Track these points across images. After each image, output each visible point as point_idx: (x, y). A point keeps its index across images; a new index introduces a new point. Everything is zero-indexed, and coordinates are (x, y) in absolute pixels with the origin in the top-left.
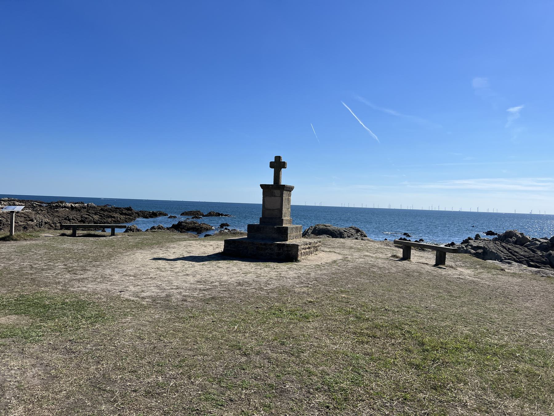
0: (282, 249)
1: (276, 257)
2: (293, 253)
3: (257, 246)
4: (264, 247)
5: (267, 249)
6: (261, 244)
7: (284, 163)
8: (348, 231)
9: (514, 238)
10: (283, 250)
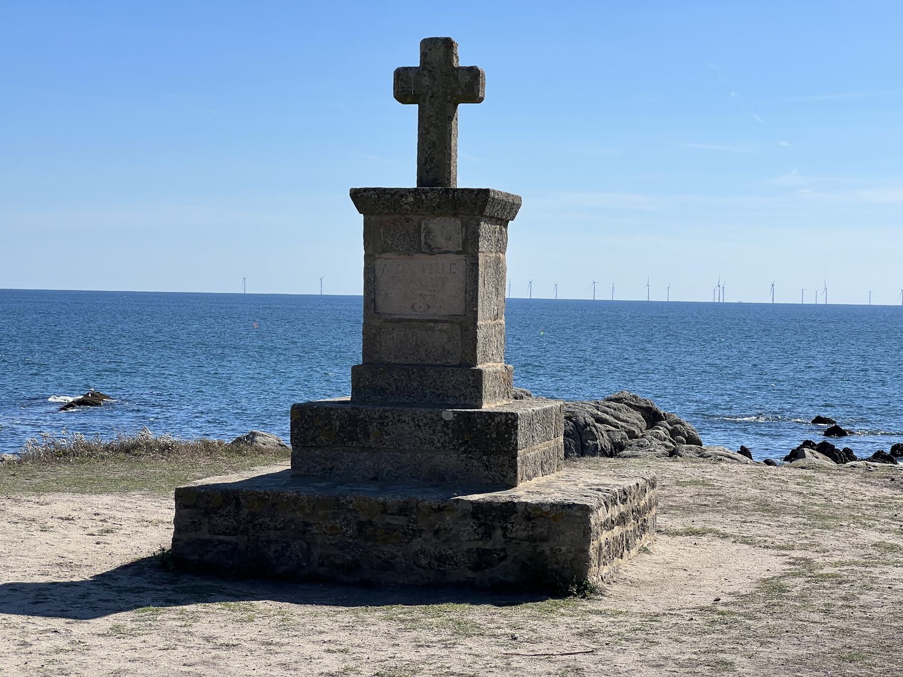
0: (499, 532)
1: (470, 574)
2: (564, 549)
3: (363, 518)
4: (400, 521)
5: (421, 531)
6: (385, 509)
7: (474, 74)
8: (611, 419)
10: (504, 535)
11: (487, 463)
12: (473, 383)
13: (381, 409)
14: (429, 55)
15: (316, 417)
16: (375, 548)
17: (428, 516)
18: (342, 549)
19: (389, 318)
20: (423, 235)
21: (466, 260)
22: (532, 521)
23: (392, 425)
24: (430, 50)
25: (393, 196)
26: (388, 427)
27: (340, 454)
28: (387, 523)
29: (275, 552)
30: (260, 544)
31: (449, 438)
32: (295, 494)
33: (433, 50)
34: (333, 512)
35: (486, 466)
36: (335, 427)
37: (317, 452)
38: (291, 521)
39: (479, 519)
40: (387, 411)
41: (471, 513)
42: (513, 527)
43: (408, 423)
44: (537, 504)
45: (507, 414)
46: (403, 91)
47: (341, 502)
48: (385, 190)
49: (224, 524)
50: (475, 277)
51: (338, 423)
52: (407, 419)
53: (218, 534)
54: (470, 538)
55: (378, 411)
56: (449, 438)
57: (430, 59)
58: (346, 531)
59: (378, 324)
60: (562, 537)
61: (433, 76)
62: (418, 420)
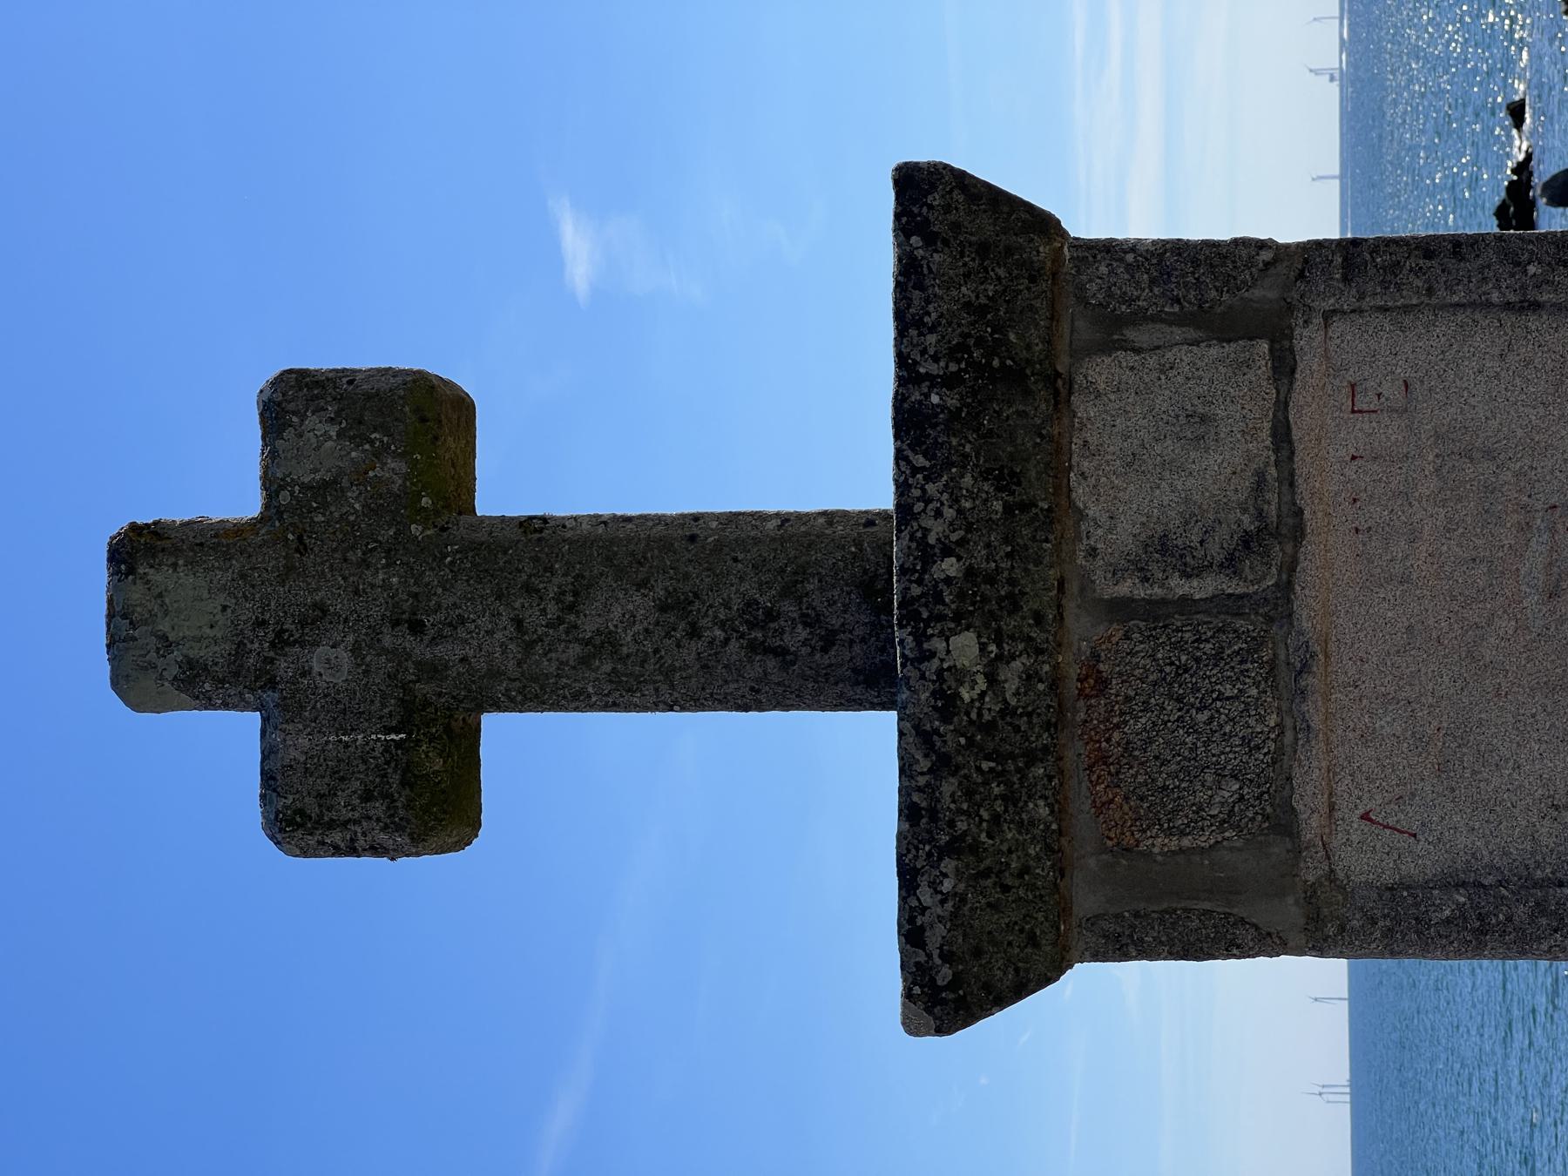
14: (197, 652)
20: (1180, 586)
21: (1328, 316)
24: (166, 644)
33: (164, 626)
46: (387, 796)
48: (909, 812)
61: (303, 624)
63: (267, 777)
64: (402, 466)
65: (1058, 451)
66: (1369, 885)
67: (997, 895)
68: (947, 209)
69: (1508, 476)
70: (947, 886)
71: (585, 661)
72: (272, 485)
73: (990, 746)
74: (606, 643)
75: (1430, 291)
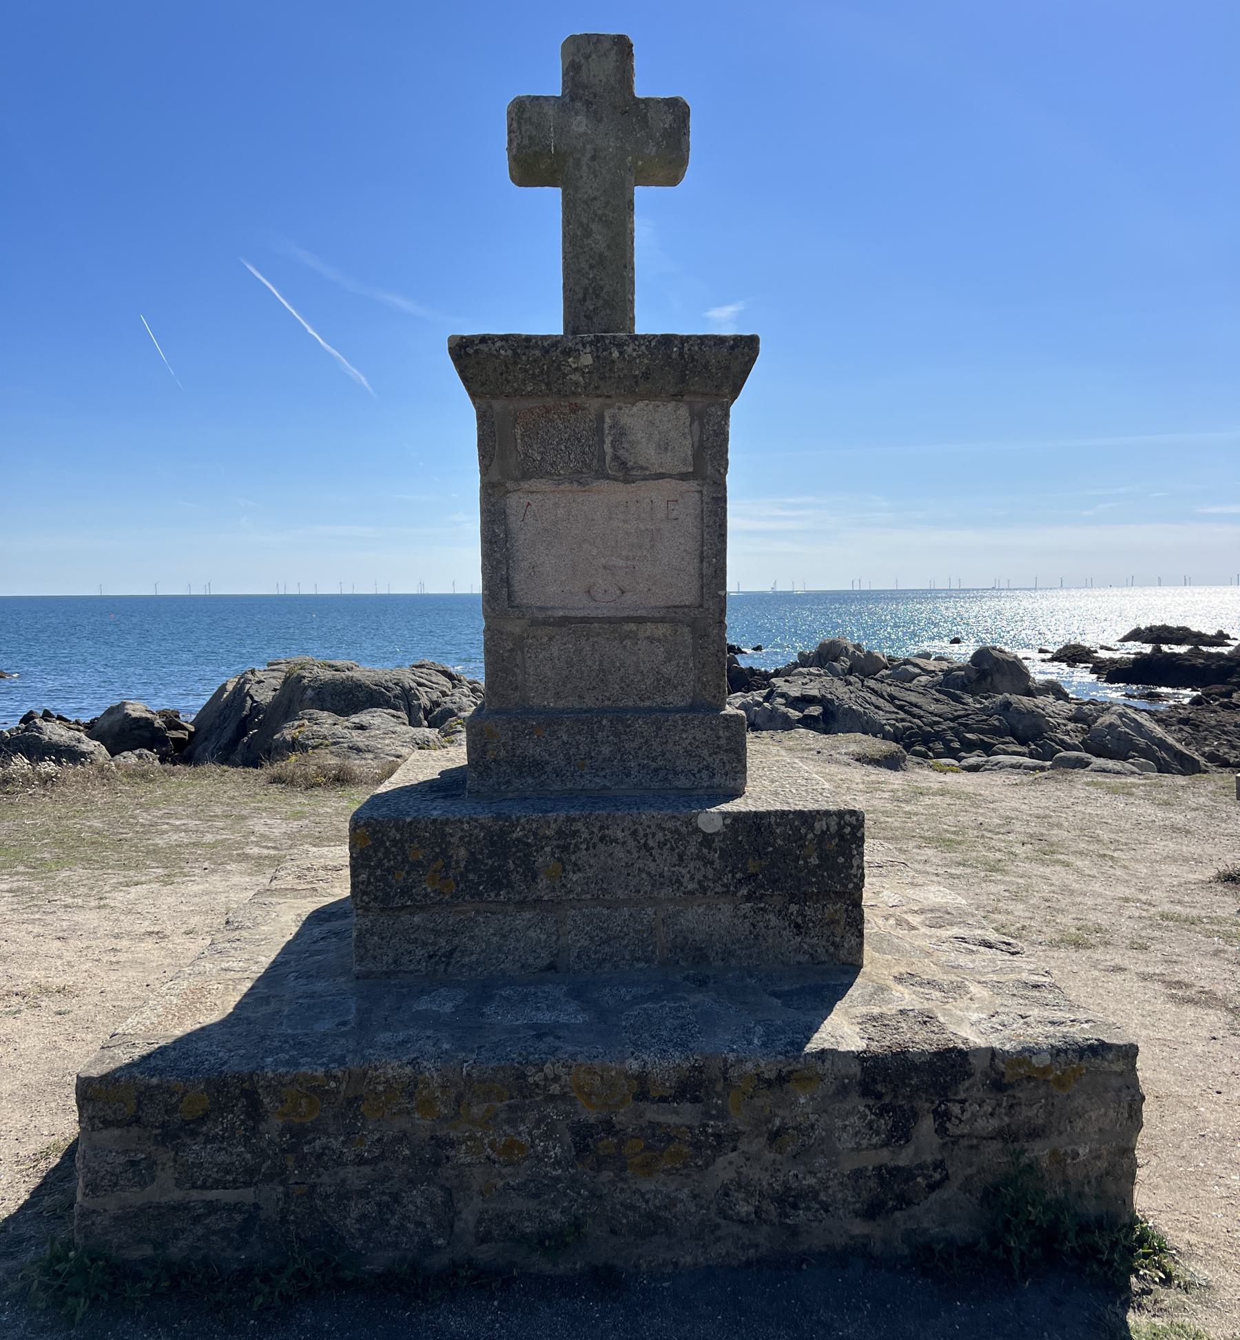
0: (927, 1124)
1: (859, 1228)
2: (1083, 1151)
3: (590, 1115)
4: (683, 1116)
5: (736, 1136)
6: (642, 1089)
8: (427, 683)
9: (844, 661)
10: (941, 1130)
11: (799, 920)
12: (728, 744)
13: (562, 815)
15: (412, 842)
16: (620, 1185)
17: (752, 1097)
18: (536, 1196)
19: (540, 615)
20: (608, 440)
21: (701, 492)
22: (1010, 1092)
23: (587, 849)
24: (587, 57)
25: (547, 352)
26: (577, 855)
27: (471, 919)
28: (650, 1122)
29: (363, 1218)
30: (319, 1202)
31: (715, 870)
32: (408, 1069)
33: (594, 56)
34: (509, 1106)
35: (797, 926)
36: (457, 862)
37: (416, 919)
38: (403, 1137)
39: (879, 1096)
40: (574, 820)
41: (860, 1084)
42: (963, 1111)
43: (624, 843)
44: (1020, 1053)
45: (840, 814)
47: (531, 1080)
48: (528, 339)
49: (219, 1160)
50: (720, 526)
51: (463, 852)
52: (620, 835)
53: (204, 1187)
54: (858, 1144)
55: (555, 821)
56: (715, 870)
57: (588, 77)
58: (546, 1149)
59: (517, 631)
60: (1079, 1124)
62: (646, 835)
63: (537, 98)
64: (653, 153)
65: (656, 396)
66: (506, 505)
67: (499, 371)
68: (743, 354)
69: (645, 553)
70: (502, 352)
71: (581, 224)
72: (646, 101)
73: (552, 369)
74: (588, 233)
75: (708, 526)
